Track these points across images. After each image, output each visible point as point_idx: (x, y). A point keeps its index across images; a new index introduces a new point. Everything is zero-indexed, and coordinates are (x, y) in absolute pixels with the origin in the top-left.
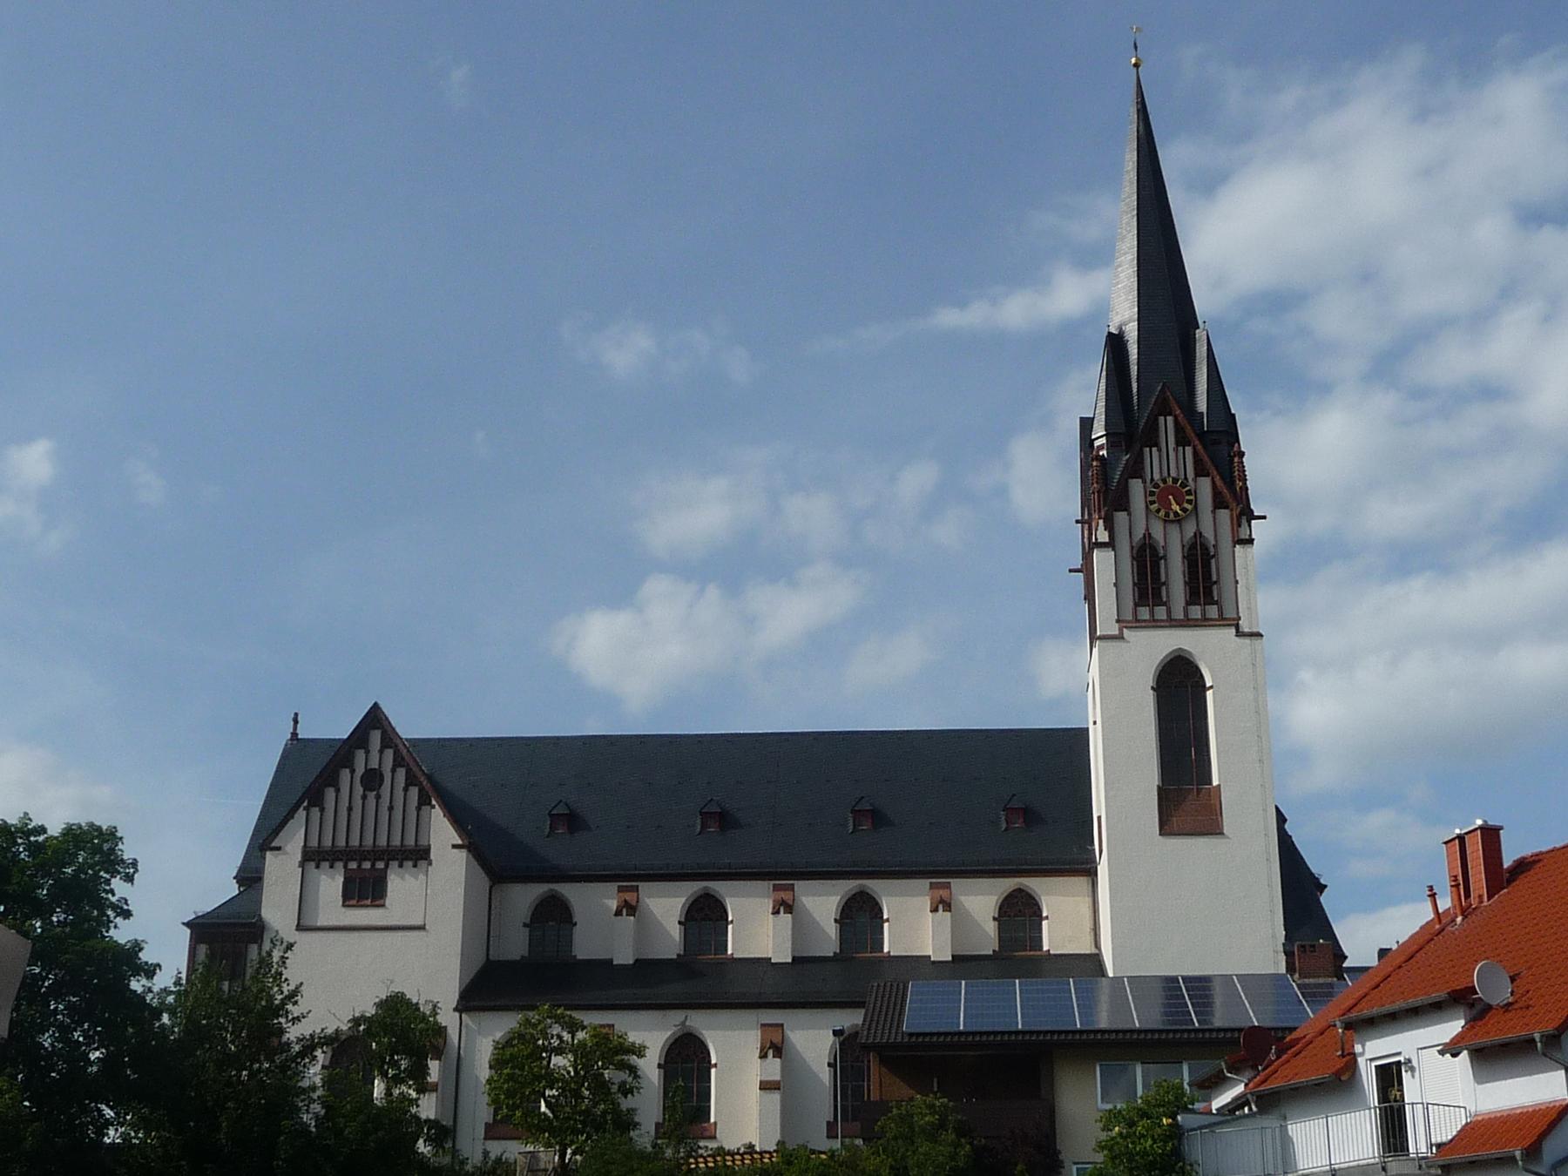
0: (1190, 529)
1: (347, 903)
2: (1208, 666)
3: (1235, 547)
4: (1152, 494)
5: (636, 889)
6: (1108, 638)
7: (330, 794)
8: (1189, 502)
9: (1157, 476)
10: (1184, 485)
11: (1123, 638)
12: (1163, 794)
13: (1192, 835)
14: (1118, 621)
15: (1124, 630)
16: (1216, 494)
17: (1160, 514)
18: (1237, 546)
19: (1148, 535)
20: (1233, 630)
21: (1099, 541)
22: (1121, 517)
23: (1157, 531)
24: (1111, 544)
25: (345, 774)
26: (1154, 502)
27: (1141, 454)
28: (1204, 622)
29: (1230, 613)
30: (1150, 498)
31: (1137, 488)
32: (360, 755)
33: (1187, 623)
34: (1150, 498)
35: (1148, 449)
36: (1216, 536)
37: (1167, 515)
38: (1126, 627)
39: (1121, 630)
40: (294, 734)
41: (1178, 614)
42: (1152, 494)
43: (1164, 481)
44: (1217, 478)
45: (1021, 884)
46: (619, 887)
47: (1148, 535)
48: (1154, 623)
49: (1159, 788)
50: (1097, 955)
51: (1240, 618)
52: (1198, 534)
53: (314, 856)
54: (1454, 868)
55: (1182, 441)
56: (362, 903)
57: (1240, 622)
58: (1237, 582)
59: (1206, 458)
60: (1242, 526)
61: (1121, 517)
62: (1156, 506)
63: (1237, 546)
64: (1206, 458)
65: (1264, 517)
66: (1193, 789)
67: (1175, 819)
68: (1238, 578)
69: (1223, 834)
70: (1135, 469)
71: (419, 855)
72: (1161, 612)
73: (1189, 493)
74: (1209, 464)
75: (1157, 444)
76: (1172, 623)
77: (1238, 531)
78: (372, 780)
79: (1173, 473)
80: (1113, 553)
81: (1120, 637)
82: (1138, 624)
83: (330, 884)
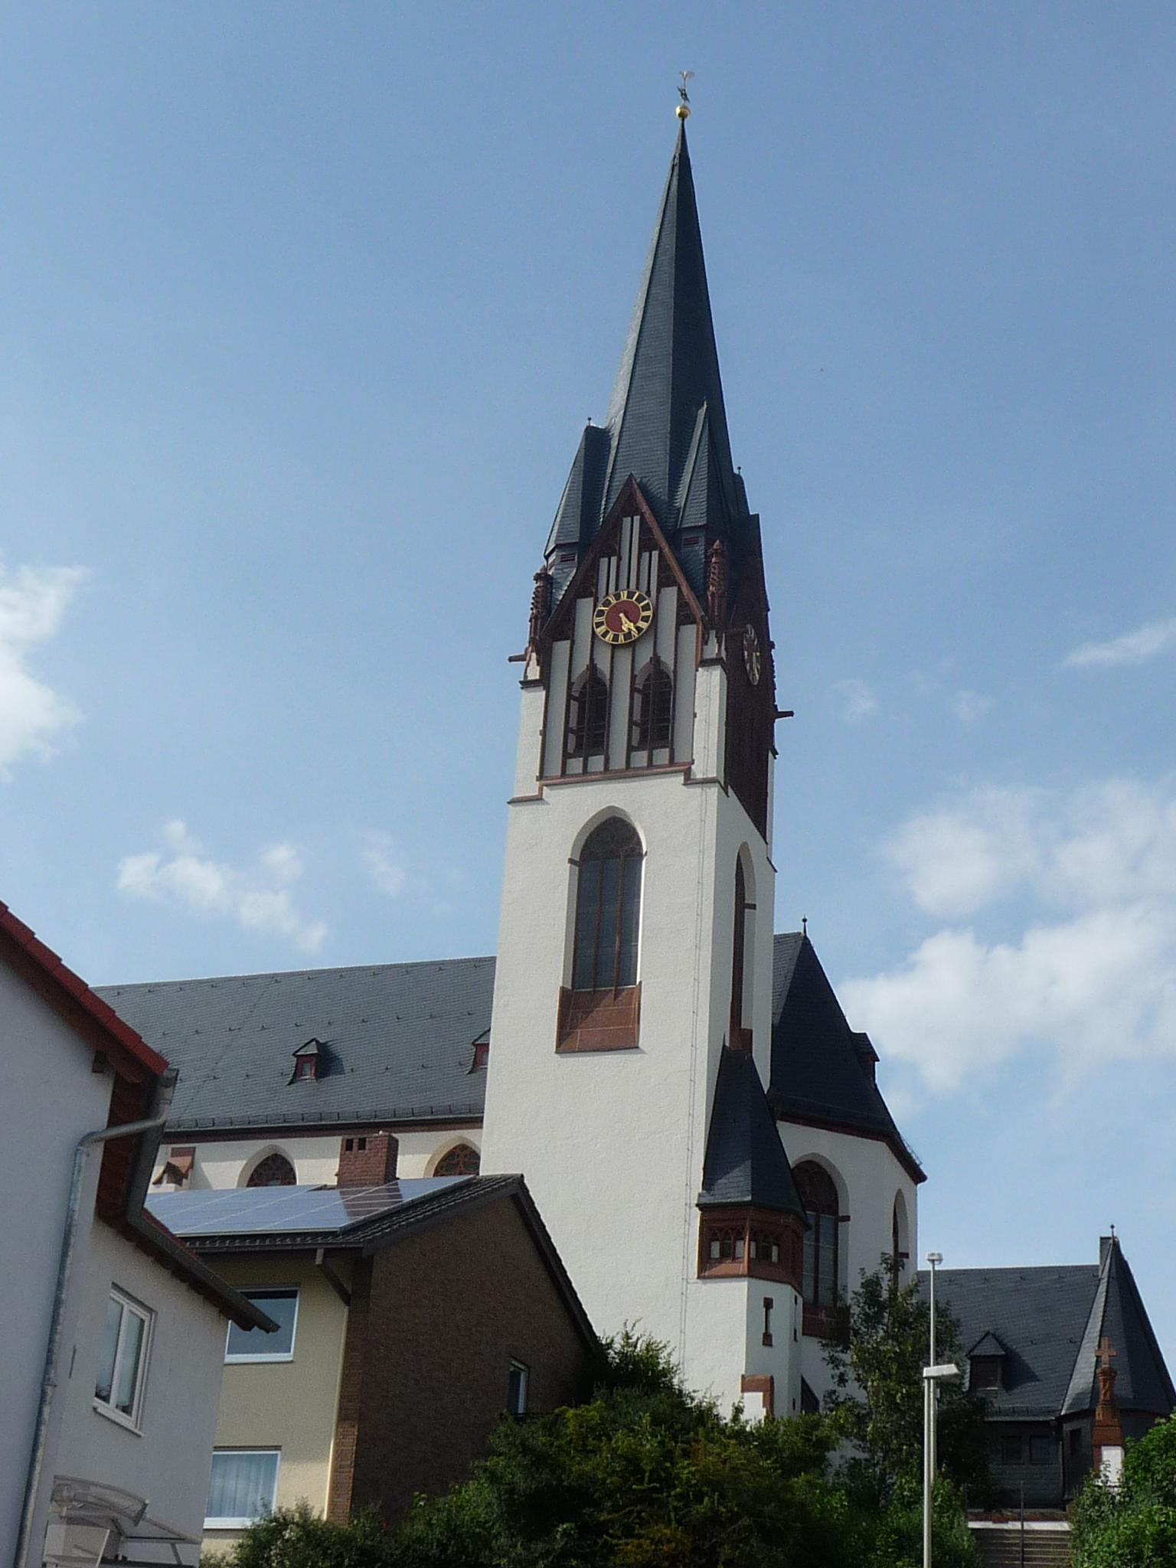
0: (645, 655)
1: (703, 1274)
2: (643, 827)
3: (697, 670)
4: (601, 613)
5: (192, 1152)
6: (526, 801)
8: (645, 619)
11: (541, 799)
12: (568, 1001)
13: (598, 1050)
14: (541, 777)
15: (545, 788)
16: (682, 605)
17: (607, 638)
18: (700, 669)
20: (681, 778)
21: (529, 678)
26: (607, 632)
27: (595, 568)
28: (651, 769)
29: (680, 758)
30: (598, 620)
33: (629, 772)
34: (598, 620)
35: (606, 559)
36: (675, 666)
37: (615, 638)
38: (546, 785)
39: (541, 790)
41: (618, 761)
42: (601, 613)
44: (685, 590)
45: (461, 1137)
46: (173, 1149)
47: (592, 667)
48: (586, 776)
49: (564, 992)
50: (107, 1141)
51: (693, 762)
52: (656, 660)
54: (740, 894)
56: (706, 1274)
57: (693, 767)
58: (695, 716)
59: (673, 564)
60: (710, 642)
61: (562, 648)
62: (603, 628)
63: (700, 669)
64: (673, 564)
65: (791, 714)
66: (611, 990)
67: (579, 1031)
68: (696, 711)
69: (638, 1047)
72: (597, 763)
74: (657, 534)
76: (609, 774)
77: (702, 649)
80: (544, 693)
81: (539, 799)
82: (565, 777)
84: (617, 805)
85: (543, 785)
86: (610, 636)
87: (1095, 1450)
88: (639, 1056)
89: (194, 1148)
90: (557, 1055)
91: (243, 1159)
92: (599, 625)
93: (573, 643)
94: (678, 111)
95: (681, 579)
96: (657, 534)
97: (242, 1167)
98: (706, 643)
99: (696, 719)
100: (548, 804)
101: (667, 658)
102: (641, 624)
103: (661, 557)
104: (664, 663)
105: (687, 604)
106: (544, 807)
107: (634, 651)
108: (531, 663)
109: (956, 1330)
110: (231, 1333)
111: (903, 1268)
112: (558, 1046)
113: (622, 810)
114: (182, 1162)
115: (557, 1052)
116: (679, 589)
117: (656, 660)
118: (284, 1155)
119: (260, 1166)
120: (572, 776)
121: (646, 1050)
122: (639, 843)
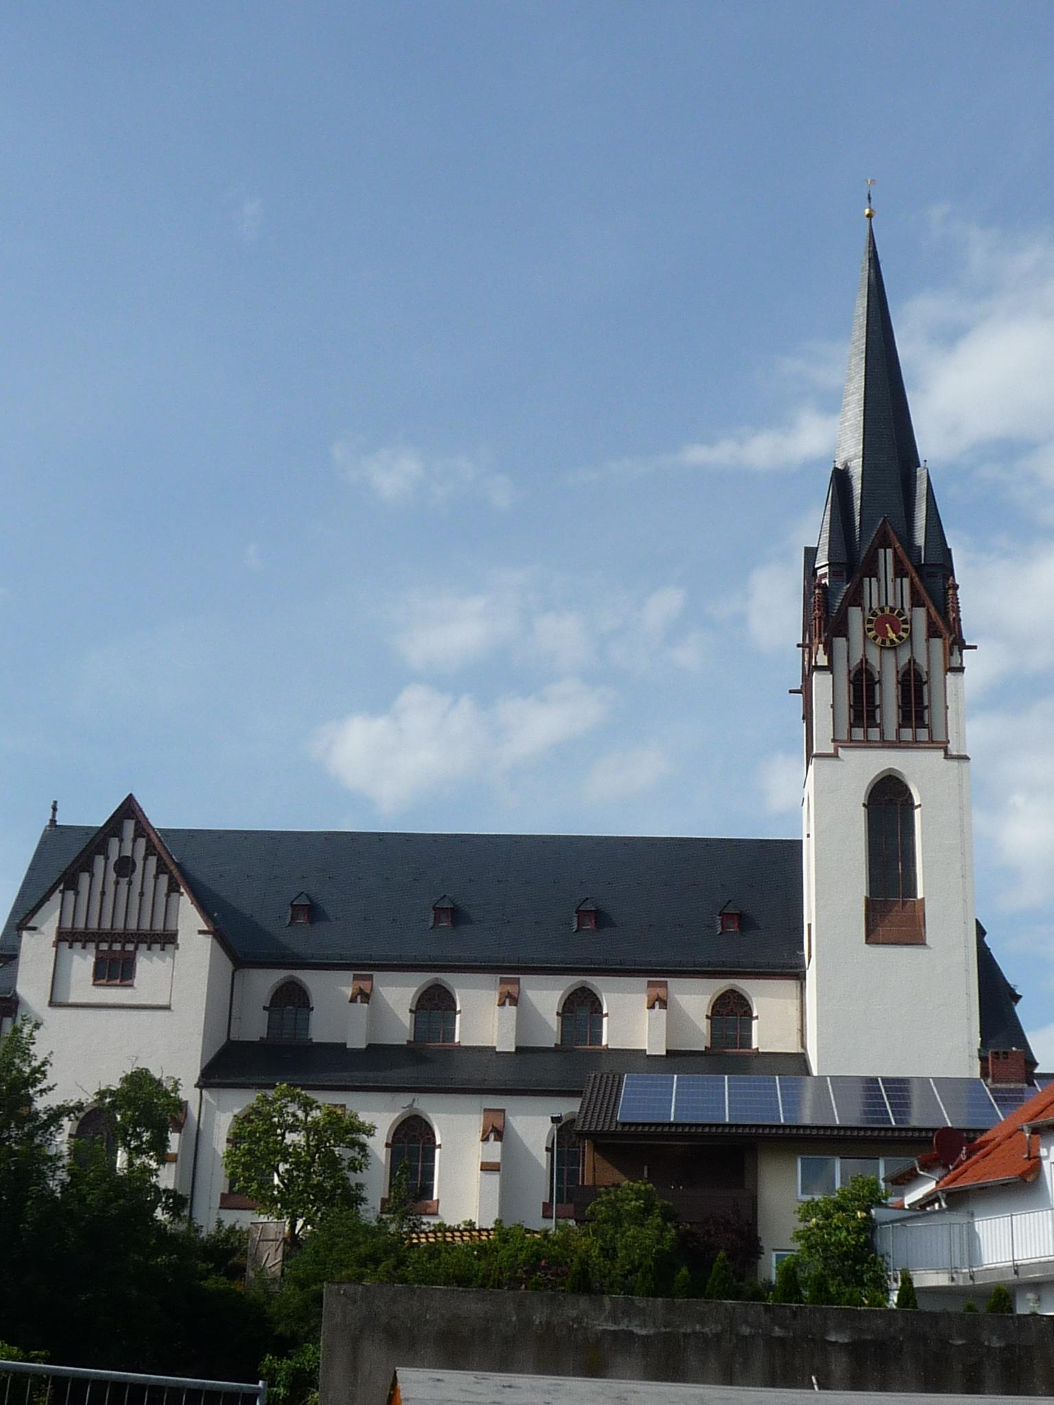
0: (905, 657)
3: (946, 674)
4: (870, 621)
7: (84, 878)
9: (875, 605)
10: (900, 614)
11: (837, 757)
14: (834, 740)
15: (839, 749)
17: (877, 641)
19: (865, 661)
20: (942, 753)
21: (819, 664)
22: (840, 643)
23: (874, 656)
24: (829, 668)
25: (99, 861)
27: (861, 584)
28: (915, 744)
29: (939, 737)
31: (855, 615)
32: (114, 842)
35: (868, 579)
36: (929, 667)
37: (883, 642)
38: (841, 747)
39: (836, 750)
40: (53, 821)
41: (891, 736)
42: (870, 621)
43: (882, 610)
44: (932, 610)
47: (865, 661)
48: (867, 744)
52: (912, 661)
53: (67, 937)
55: (900, 573)
57: (949, 746)
61: (840, 643)
68: (948, 704)
69: (925, 944)
70: (855, 598)
71: (166, 939)
72: (874, 734)
73: (905, 622)
74: (908, 565)
75: (876, 575)
76: (885, 744)
78: (125, 867)
79: (891, 603)
81: (835, 756)
82: (852, 743)
83: (82, 963)
84: (896, 768)
85: (839, 746)
86: (879, 640)
87: (924, 1305)
88: (926, 951)
89: (519, 979)
90: (867, 946)
91: (560, 990)
92: (870, 630)
93: (848, 640)
94: (867, 211)
95: (929, 602)
96: (908, 565)
97: (559, 996)
98: (952, 655)
99: (949, 711)
100: (843, 761)
101: (922, 661)
102: (902, 634)
103: (912, 584)
104: (918, 665)
105: (935, 623)
106: (840, 763)
107: (896, 654)
108: (819, 652)
109: (232, 1244)
110: (935, 1096)
111: (983, 1131)
112: (867, 940)
113: (897, 771)
114: (365, 985)
115: (867, 943)
116: (928, 610)
117: (912, 661)
118: (590, 987)
119: (571, 995)
120: (856, 741)
121: (932, 946)
122: (910, 795)
